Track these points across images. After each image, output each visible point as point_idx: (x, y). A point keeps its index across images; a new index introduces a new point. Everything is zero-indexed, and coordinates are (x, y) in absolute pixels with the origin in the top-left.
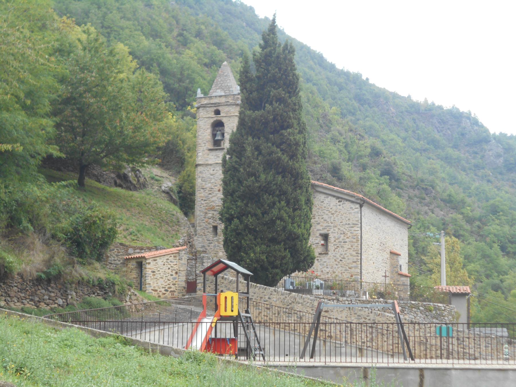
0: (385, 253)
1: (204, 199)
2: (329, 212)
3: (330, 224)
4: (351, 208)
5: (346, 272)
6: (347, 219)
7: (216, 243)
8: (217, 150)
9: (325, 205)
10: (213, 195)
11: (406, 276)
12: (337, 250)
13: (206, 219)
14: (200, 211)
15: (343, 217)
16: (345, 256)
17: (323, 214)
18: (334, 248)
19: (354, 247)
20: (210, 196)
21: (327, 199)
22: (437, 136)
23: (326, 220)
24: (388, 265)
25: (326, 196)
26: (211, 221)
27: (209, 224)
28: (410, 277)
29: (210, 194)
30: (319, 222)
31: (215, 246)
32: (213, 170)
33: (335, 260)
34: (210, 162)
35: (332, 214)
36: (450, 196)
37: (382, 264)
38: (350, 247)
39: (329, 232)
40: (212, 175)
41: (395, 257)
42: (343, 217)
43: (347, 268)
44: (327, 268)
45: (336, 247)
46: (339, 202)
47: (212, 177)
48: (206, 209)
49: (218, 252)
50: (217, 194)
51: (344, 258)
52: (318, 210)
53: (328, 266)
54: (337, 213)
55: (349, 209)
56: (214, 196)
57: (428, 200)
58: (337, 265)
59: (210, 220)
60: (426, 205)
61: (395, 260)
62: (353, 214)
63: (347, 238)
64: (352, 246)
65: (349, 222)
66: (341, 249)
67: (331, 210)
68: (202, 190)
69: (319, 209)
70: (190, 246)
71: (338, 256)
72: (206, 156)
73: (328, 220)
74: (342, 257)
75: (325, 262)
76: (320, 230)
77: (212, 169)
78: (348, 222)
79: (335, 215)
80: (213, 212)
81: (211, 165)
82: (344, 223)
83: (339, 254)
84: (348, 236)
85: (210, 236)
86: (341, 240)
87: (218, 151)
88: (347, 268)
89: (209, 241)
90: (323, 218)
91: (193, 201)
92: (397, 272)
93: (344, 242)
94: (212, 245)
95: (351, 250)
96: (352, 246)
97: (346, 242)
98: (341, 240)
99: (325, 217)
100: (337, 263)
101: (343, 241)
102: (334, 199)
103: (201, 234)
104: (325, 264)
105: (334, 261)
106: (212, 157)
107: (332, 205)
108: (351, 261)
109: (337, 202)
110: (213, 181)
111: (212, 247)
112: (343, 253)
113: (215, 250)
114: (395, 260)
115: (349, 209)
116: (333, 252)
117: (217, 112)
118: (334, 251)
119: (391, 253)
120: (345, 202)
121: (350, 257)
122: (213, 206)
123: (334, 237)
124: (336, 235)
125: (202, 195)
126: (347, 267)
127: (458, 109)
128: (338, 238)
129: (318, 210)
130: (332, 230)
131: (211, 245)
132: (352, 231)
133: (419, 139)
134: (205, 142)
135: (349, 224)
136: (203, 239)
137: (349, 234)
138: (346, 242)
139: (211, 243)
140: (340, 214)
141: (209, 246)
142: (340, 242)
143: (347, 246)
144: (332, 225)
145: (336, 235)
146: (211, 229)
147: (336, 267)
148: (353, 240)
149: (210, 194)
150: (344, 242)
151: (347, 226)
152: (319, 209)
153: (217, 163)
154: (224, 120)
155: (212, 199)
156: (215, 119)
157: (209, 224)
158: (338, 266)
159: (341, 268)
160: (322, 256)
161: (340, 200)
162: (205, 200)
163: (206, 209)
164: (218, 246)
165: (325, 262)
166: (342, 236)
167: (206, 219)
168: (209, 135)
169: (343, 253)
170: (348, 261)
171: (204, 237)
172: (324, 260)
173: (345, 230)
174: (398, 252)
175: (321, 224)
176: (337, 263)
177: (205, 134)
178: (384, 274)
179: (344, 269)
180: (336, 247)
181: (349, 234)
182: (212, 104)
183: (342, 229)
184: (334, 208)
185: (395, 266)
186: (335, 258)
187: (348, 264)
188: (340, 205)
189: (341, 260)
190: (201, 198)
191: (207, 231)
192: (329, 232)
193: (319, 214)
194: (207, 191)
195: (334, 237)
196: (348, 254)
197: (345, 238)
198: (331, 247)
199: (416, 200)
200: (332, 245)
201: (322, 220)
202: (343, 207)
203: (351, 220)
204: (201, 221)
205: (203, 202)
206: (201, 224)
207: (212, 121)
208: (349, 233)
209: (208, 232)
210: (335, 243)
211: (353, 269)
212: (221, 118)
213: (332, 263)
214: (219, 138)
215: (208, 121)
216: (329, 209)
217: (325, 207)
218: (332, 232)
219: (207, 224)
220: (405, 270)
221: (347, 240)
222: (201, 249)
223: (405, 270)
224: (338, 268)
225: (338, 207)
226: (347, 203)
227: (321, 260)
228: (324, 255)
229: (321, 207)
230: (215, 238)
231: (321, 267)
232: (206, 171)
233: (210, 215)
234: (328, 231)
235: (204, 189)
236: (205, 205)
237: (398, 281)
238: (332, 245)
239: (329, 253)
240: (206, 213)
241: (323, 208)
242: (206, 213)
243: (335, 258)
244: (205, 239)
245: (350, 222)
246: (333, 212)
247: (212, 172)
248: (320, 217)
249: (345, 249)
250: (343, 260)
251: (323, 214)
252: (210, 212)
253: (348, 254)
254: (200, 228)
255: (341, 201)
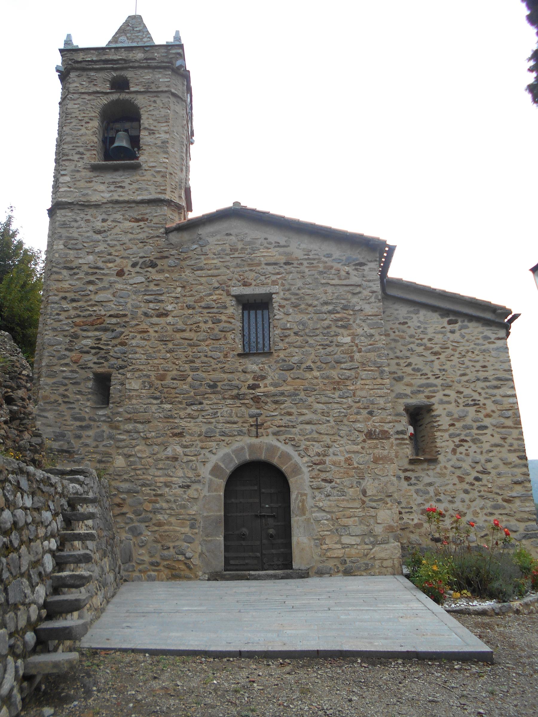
1: (70, 295)
2: (427, 349)
3: (432, 381)
4: (486, 338)
5: (497, 512)
6: (478, 365)
7: (105, 427)
8: (116, 169)
9: (411, 331)
10: (101, 285)
12: (461, 449)
13: (74, 355)
14: (54, 329)
15: (466, 360)
16: (489, 466)
17: (408, 354)
18: (452, 446)
19: (509, 440)
20: (91, 287)
21: (415, 316)
23: (418, 370)
25: (412, 309)
26: (90, 359)
27: (84, 367)
29: (90, 282)
30: (400, 374)
31: (99, 437)
32: (104, 221)
33: (461, 479)
34: (95, 198)
35: (435, 354)
38: (497, 439)
39: (433, 400)
40: (99, 232)
42: (466, 360)
43: (500, 502)
44: (439, 501)
45: (457, 440)
46: (450, 322)
47: (99, 237)
48: (76, 325)
49: (109, 455)
50: (111, 284)
51: (485, 472)
52: (393, 345)
53: (442, 497)
54: (449, 352)
55: (481, 341)
56: (104, 289)
58: (466, 492)
59: (87, 357)
62: (493, 353)
63: (488, 416)
64: (504, 439)
65: (485, 374)
66: (474, 448)
67: (429, 345)
68: (65, 272)
69: (395, 341)
70: (13, 417)
71: (466, 466)
72: (82, 184)
73: (426, 370)
74: (479, 468)
75: (430, 484)
76: (406, 395)
77: (100, 218)
78: (482, 375)
79: (442, 357)
80: (97, 333)
81: (97, 206)
82: (471, 376)
83: (469, 460)
84: (488, 411)
85: (86, 405)
86: (468, 421)
87: (120, 173)
88: (500, 502)
89: (82, 419)
90: (409, 364)
91: (35, 342)
93: (479, 428)
94: (91, 433)
95: (504, 450)
96: (504, 439)
97: (486, 427)
98: (468, 421)
99: (415, 360)
100: (467, 487)
101: (475, 425)
102: (435, 317)
103: (53, 398)
104: (431, 489)
105: (456, 481)
106: (102, 187)
107: (430, 331)
108: (506, 480)
109: (445, 324)
110: (101, 247)
111: (88, 441)
112: (482, 458)
113: (101, 449)
115: (481, 341)
116: (450, 456)
117: (120, 85)
118: (454, 451)
120: (466, 323)
121: (503, 469)
122: (99, 317)
123: (449, 414)
124: (451, 407)
125: (65, 285)
126: (500, 498)
128: (461, 418)
129: (393, 345)
130: (439, 396)
131: (85, 433)
132: (498, 398)
134: (81, 150)
135: (486, 379)
136: (61, 415)
137: (490, 406)
138: (486, 427)
139: (88, 427)
140: (457, 355)
141: (79, 437)
142: (466, 427)
143: (488, 437)
144: (438, 382)
145: (451, 407)
146: (90, 384)
147: (466, 497)
148: (503, 420)
149: (90, 282)
150: (479, 428)
151: (480, 384)
152: (395, 341)
153: (117, 202)
154: (140, 101)
155: (97, 298)
156: (115, 97)
157: (84, 367)
158: (471, 496)
159: (480, 503)
160: (418, 467)
161: (452, 318)
162: (73, 300)
163: (76, 325)
164: (111, 437)
165: (430, 484)
166: (472, 410)
167: (74, 355)
168: (94, 133)
169: (482, 458)
170: (500, 481)
171: (63, 407)
172: (427, 480)
173: (476, 396)
175: (407, 379)
176: (467, 487)
177: (84, 130)
179: (489, 504)
180: (457, 440)
181: (490, 406)
182: (106, 61)
183: (467, 392)
184: (439, 338)
186: (458, 473)
187: (501, 488)
188: (452, 332)
189: (477, 479)
190: (63, 294)
191: (75, 389)
192: (433, 400)
193: (399, 354)
194: (81, 275)
195: (449, 414)
196: (496, 461)
197: (481, 415)
198: (443, 442)
200: (446, 435)
201: (409, 370)
202: (463, 337)
203: (490, 368)
204: (55, 361)
205: (65, 305)
206: (56, 369)
207: (104, 100)
208: (489, 402)
209: (80, 393)
210: (452, 430)
211: (518, 503)
212: (132, 96)
213: (450, 487)
214: (122, 142)
215: (95, 103)
216: (425, 341)
217: (411, 336)
218: (442, 402)
219: (75, 367)
221: (487, 422)
222: (56, 445)
224: (472, 501)
225: (449, 335)
226: (472, 325)
227: (417, 478)
228: (425, 466)
229: (403, 338)
230: (101, 412)
231: (420, 500)
232: (83, 224)
233: (89, 342)
234: (428, 397)
235: (72, 269)
236: (73, 313)
238: (446, 435)
239: (441, 458)
240: (75, 336)
241: (408, 339)
242: (75, 336)
243: (458, 473)
244: (68, 415)
245: (489, 374)
246: (437, 349)
247: (99, 225)
248: (401, 361)
249: (486, 446)
250: (484, 477)
251: (408, 354)
252: (90, 334)
253: (496, 461)
254: (50, 381)
255: (456, 322)
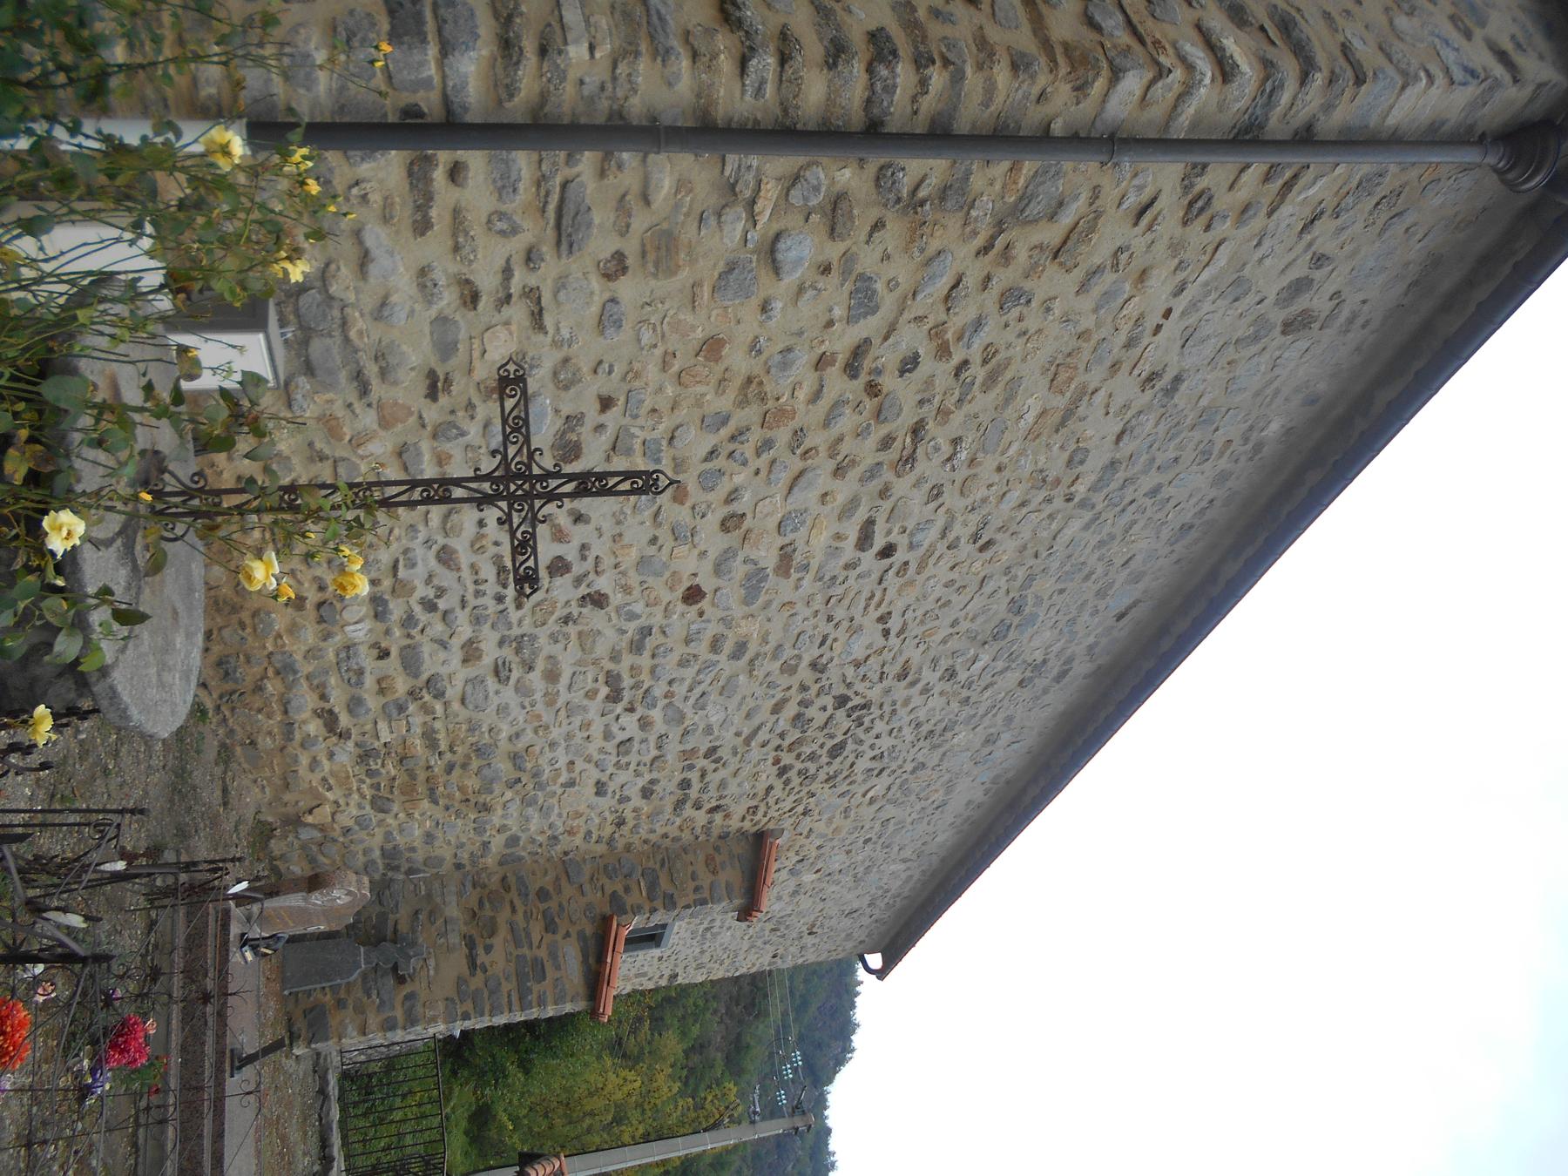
0: (768, 774)
11: (595, 980)
22: (813, 1009)
24: (667, 825)
28: (594, 1013)
36: (748, 1047)
37: (673, 749)
41: (732, 875)
57: (737, 1010)
60: (728, 1008)
61: (705, 879)
92: (618, 905)
114: (705, 879)
119: (759, 842)
127: (853, 1032)
133: (806, 981)
174: (771, 902)
178: (568, 532)
185: (664, 884)
199: (735, 990)
220: (633, 971)
223: (633, 971)
237: (550, 927)
